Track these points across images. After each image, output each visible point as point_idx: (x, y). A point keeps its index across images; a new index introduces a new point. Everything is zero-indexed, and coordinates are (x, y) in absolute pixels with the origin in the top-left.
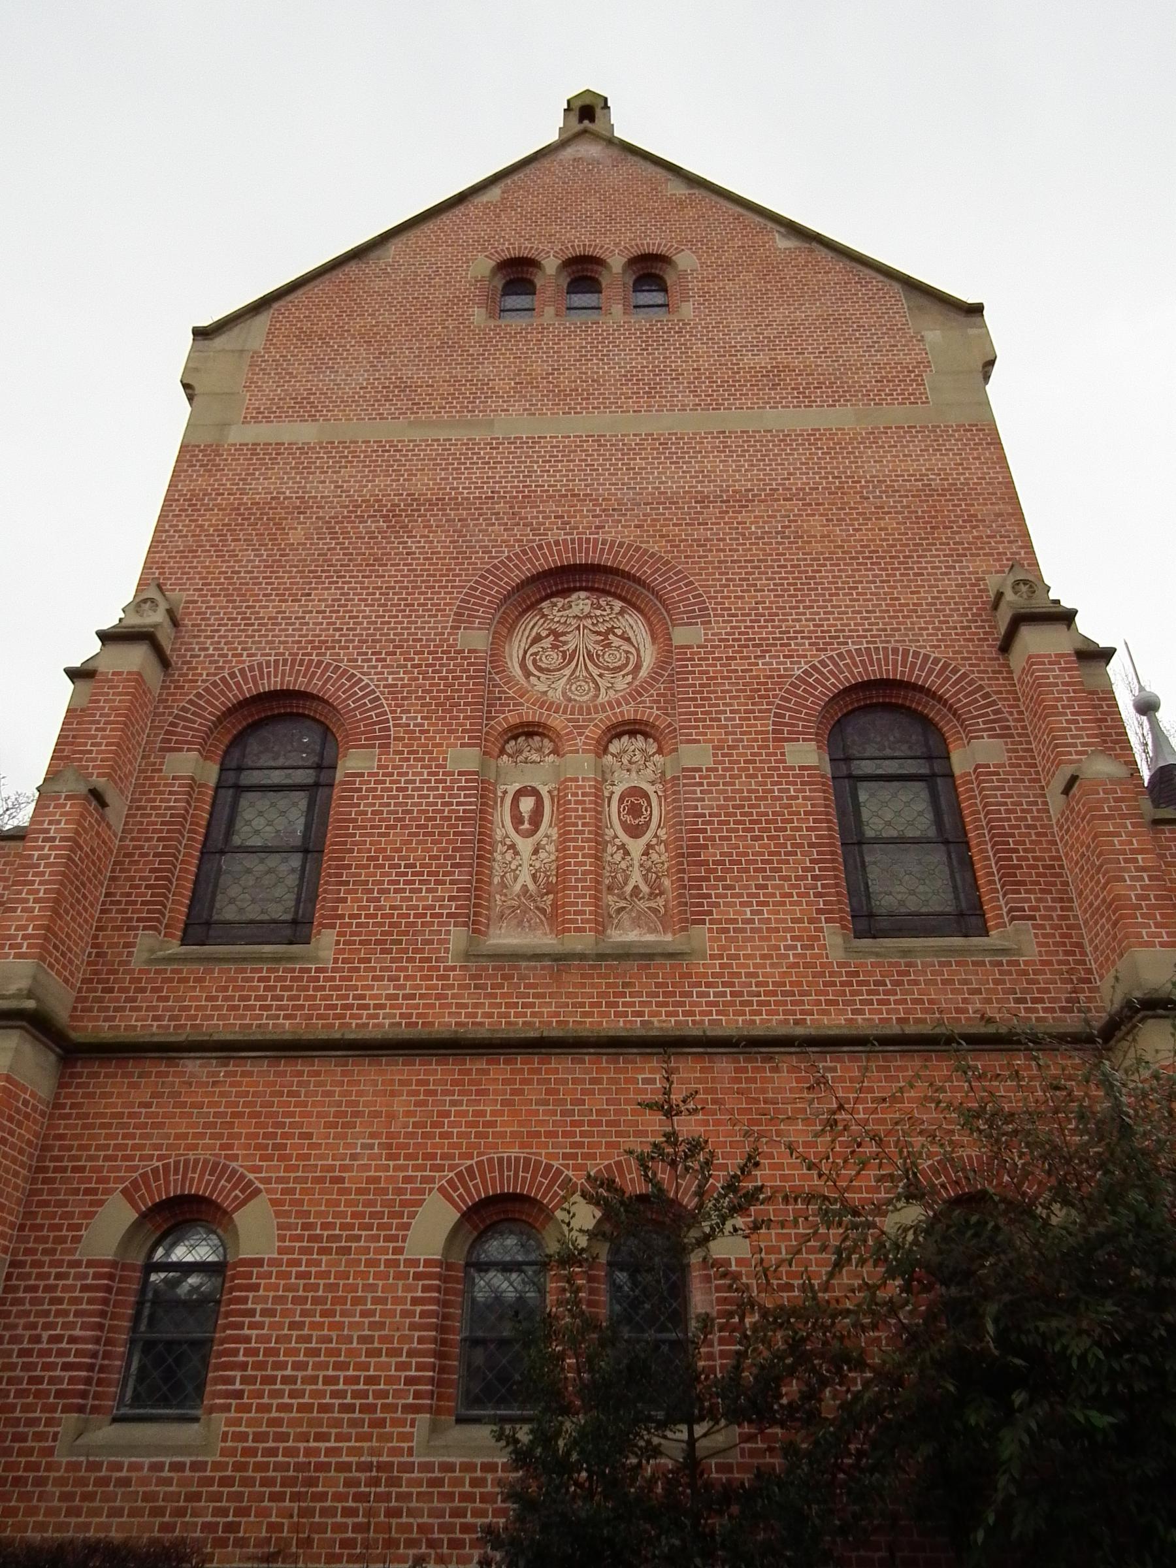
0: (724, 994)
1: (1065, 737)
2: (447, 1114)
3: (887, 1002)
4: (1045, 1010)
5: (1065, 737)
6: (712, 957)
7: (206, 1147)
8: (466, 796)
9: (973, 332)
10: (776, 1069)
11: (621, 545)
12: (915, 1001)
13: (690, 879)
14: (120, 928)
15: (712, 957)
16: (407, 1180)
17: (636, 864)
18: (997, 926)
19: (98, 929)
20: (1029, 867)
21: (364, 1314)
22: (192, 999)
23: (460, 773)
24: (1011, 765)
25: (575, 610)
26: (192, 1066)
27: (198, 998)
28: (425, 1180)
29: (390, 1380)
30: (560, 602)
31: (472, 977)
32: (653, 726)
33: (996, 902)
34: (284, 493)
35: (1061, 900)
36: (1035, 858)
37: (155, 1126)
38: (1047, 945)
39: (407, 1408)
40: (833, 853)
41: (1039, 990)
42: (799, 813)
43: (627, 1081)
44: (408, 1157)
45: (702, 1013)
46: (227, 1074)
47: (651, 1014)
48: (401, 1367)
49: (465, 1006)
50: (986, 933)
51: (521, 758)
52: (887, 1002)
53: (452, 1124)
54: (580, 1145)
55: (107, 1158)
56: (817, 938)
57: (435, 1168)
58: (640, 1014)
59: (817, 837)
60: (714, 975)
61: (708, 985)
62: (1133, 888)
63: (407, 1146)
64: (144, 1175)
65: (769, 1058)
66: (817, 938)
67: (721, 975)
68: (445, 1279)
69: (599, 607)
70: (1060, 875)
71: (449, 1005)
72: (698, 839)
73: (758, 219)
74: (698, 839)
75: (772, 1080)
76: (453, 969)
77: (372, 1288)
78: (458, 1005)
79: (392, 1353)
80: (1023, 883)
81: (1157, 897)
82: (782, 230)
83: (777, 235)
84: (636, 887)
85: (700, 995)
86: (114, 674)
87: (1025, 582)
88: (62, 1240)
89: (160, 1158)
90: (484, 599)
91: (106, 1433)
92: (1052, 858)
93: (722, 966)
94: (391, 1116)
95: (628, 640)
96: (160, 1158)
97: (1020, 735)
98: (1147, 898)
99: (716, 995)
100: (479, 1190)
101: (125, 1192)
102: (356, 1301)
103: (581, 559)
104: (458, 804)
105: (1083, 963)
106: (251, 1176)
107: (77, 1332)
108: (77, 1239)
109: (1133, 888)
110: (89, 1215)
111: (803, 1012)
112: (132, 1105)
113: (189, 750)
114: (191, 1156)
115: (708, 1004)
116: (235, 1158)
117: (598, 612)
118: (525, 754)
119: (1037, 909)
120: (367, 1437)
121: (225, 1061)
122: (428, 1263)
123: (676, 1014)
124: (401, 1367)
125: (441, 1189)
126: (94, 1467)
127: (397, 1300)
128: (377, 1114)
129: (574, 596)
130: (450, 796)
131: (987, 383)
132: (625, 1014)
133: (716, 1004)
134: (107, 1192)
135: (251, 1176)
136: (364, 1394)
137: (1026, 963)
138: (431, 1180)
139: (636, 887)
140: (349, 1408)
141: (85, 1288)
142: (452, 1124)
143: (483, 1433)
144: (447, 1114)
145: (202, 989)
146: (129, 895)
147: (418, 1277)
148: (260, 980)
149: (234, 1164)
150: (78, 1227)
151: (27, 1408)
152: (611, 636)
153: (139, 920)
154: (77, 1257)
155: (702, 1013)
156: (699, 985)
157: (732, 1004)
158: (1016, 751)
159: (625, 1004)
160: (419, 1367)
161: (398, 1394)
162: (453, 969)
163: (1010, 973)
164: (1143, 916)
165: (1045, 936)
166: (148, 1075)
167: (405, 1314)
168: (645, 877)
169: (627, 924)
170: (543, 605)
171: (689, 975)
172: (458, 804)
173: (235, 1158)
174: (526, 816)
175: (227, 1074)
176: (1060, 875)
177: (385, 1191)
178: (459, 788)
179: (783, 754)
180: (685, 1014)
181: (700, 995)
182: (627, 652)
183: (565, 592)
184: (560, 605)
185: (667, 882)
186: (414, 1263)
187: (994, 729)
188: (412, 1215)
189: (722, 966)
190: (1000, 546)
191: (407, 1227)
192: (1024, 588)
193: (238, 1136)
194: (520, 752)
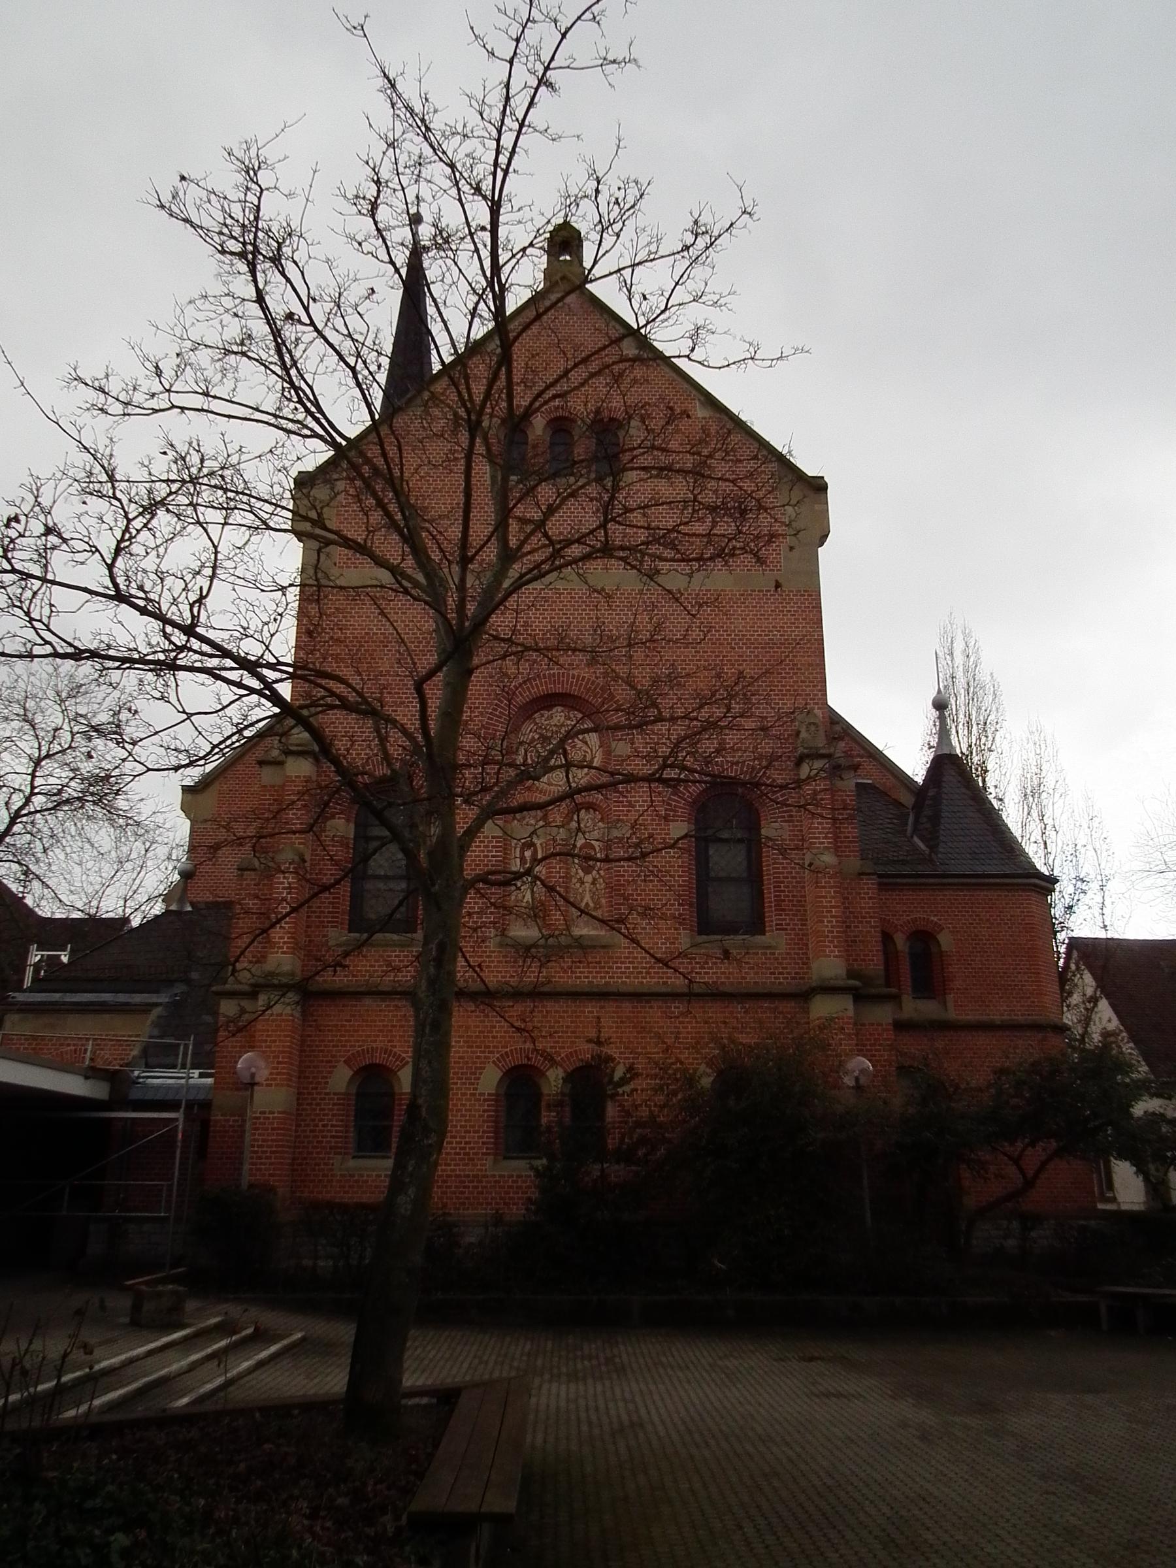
0: (629, 968)
1: (814, 833)
2: (495, 1027)
3: (709, 973)
4: (784, 978)
5: (814, 833)
6: (625, 948)
7: (381, 1041)
8: (496, 851)
9: (817, 507)
10: (651, 1007)
11: (584, 678)
12: (723, 973)
13: (616, 904)
14: (318, 927)
15: (625, 948)
16: (478, 1057)
17: (587, 889)
18: (770, 931)
19: (308, 927)
20: (789, 901)
21: (462, 1116)
22: (362, 966)
23: (493, 837)
24: (790, 840)
25: (554, 721)
26: (368, 1001)
27: (366, 966)
28: (486, 1057)
29: (475, 1143)
30: (546, 713)
31: (503, 957)
32: (599, 806)
33: (771, 917)
34: (372, 629)
35: (802, 920)
36: (793, 896)
37: (355, 1031)
38: (790, 944)
39: (483, 1154)
40: (690, 846)
41: (783, 968)
42: (674, 866)
43: (580, 1012)
44: (477, 1047)
45: (618, 977)
46: (387, 1006)
47: (593, 977)
48: (479, 1137)
49: (501, 972)
50: (763, 933)
51: (525, 822)
52: (709, 973)
53: (497, 1032)
54: (558, 1042)
55: (333, 1046)
56: (677, 939)
57: (490, 1052)
58: (587, 977)
59: (683, 881)
60: (625, 957)
61: (622, 963)
62: (827, 926)
63: (476, 1042)
64: (353, 1054)
65: (648, 1002)
66: (677, 939)
67: (628, 958)
68: (496, 1101)
69: (569, 718)
70: (803, 906)
71: (493, 972)
72: (620, 880)
73: (686, 385)
74: (620, 880)
75: (649, 1012)
76: (494, 952)
77: (464, 1105)
78: (497, 972)
79: (475, 1132)
80: (784, 910)
81: (837, 932)
82: (702, 399)
83: (697, 402)
84: (587, 903)
85: (617, 968)
86: (296, 777)
87: (814, 724)
88: (319, 1083)
89: (360, 1046)
90: (500, 712)
91: (352, 1163)
92: (801, 896)
93: (629, 953)
94: (468, 1027)
95: (586, 743)
96: (360, 1046)
97: (798, 821)
98: (833, 932)
99: (625, 968)
100: (511, 1062)
101: (345, 1061)
102: (458, 1111)
103: (559, 689)
104: (493, 856)
105: (806, 954)
106: (404, 1055)
107: (334, 1123)
108: (327, 1083)
109: (827, 926)
110: (330, 1072)
111: (667, 978)
112: (342, 1021)
113: (339, 818)
114: (374, 1045)
115: (621, 973)
116: (395, 1046)
117: (569, 722)
118: (527, 820)
119: (788, 925)
120: (467, 1165)
121: (383, 1000)
122: (489, 1094)
123: (605, 977)
124: (479, 1137)
125: (494, 1062)
126: (352, 1176)
127: (476, 1110)
128: (461, 1026)
129: (554, 710)
130: (488, 851)
131: (822, 545)
132: (580, 977)
133: (625, 973)
134: (338, 1061)
135: (404, 1055)
136: (464, 1148)
137: (779, 954)
138: (489, 1058)
139: (587, 903)
140: (459, 1154)
141: (334, 1104)
142: (497, 1032)
143: (522, 1164)
144: (495, 1027)
145: (367, 961)
146: (320, 907)
147: (485, 1100)
148: (396, 956)
149: (395, 1050)
150: (326, 1078)
151: (318, 1153)
152: (576, 740)
153: (328, 922)
154: (328, 1091)
155: (618, 977)
156: (617, 963)
157: (633, 973)
158: (793, 831)
159: (580, 972)
160: (488, 1137)
161: (479, 1148)
162: (494, 952)
163: (770, 959)
164: (829, 942)
165: (791, 939)
166: (347, 1006)
167: (480, 1116)
168: (592, 898)
169: (582, 924)
170: (536, 715)
171: (612, 958)
172: (493, 856)
173: (395, 1046)
174: (528, 859)
175: (387, 1006)
176: (803, 906)
177: (467, 1063)
178: (493, 847)
179: (669, 829)
180: (610, 977)
181: (617, 968)
182: (585, 752)
183: (549, 708)
184: (546, 716)
185: (603, 901)
186: (482, 1094)
187: (784, 817)
188: (481, 1074)
189: (629, 953)
190: (808, 689)
191: (479, 1079)
192: (813, 728)
193: (395, 1036)
194: (524, 818)
